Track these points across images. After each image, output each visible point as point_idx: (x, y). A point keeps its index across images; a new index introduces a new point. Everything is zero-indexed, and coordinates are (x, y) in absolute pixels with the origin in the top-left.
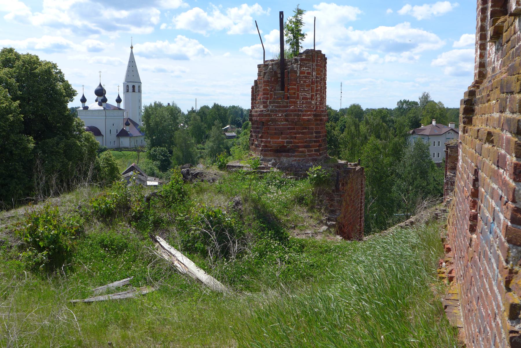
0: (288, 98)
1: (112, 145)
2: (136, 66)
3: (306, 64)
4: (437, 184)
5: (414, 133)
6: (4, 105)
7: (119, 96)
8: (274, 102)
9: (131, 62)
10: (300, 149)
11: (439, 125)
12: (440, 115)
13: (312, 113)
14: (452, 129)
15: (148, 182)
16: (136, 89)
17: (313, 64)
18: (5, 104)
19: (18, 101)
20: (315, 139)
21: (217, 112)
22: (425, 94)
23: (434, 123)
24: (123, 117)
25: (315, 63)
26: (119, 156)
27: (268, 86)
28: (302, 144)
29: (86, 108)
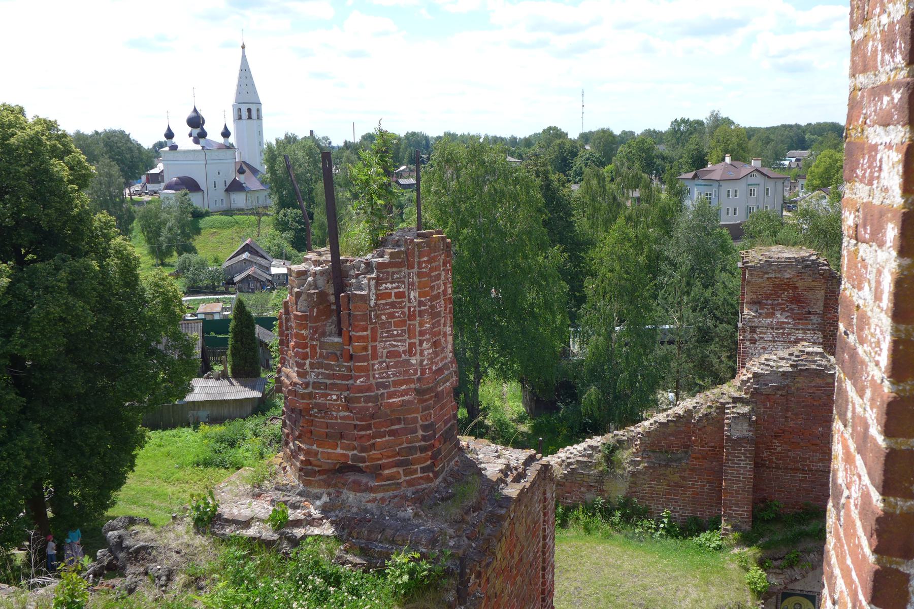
0: (351, 357)
1: (220, 206)
2: (251, 77)
3: (393, 273)
4: (729, 294)
5: (695, 176)
7: (226, 128)
8: (320, 366)
10: (387, 472)
11: (736, 163)
12: (738, 145)
13: (413, 386)
14: (757, 170)
17: (409, 274)
20: (423, 443)
22: (715, 114)
23: (728, 160)
24: (234, 161)
25: (416, 270)
27: (305, 328)
28: (391, 460)
29: (174, 148)
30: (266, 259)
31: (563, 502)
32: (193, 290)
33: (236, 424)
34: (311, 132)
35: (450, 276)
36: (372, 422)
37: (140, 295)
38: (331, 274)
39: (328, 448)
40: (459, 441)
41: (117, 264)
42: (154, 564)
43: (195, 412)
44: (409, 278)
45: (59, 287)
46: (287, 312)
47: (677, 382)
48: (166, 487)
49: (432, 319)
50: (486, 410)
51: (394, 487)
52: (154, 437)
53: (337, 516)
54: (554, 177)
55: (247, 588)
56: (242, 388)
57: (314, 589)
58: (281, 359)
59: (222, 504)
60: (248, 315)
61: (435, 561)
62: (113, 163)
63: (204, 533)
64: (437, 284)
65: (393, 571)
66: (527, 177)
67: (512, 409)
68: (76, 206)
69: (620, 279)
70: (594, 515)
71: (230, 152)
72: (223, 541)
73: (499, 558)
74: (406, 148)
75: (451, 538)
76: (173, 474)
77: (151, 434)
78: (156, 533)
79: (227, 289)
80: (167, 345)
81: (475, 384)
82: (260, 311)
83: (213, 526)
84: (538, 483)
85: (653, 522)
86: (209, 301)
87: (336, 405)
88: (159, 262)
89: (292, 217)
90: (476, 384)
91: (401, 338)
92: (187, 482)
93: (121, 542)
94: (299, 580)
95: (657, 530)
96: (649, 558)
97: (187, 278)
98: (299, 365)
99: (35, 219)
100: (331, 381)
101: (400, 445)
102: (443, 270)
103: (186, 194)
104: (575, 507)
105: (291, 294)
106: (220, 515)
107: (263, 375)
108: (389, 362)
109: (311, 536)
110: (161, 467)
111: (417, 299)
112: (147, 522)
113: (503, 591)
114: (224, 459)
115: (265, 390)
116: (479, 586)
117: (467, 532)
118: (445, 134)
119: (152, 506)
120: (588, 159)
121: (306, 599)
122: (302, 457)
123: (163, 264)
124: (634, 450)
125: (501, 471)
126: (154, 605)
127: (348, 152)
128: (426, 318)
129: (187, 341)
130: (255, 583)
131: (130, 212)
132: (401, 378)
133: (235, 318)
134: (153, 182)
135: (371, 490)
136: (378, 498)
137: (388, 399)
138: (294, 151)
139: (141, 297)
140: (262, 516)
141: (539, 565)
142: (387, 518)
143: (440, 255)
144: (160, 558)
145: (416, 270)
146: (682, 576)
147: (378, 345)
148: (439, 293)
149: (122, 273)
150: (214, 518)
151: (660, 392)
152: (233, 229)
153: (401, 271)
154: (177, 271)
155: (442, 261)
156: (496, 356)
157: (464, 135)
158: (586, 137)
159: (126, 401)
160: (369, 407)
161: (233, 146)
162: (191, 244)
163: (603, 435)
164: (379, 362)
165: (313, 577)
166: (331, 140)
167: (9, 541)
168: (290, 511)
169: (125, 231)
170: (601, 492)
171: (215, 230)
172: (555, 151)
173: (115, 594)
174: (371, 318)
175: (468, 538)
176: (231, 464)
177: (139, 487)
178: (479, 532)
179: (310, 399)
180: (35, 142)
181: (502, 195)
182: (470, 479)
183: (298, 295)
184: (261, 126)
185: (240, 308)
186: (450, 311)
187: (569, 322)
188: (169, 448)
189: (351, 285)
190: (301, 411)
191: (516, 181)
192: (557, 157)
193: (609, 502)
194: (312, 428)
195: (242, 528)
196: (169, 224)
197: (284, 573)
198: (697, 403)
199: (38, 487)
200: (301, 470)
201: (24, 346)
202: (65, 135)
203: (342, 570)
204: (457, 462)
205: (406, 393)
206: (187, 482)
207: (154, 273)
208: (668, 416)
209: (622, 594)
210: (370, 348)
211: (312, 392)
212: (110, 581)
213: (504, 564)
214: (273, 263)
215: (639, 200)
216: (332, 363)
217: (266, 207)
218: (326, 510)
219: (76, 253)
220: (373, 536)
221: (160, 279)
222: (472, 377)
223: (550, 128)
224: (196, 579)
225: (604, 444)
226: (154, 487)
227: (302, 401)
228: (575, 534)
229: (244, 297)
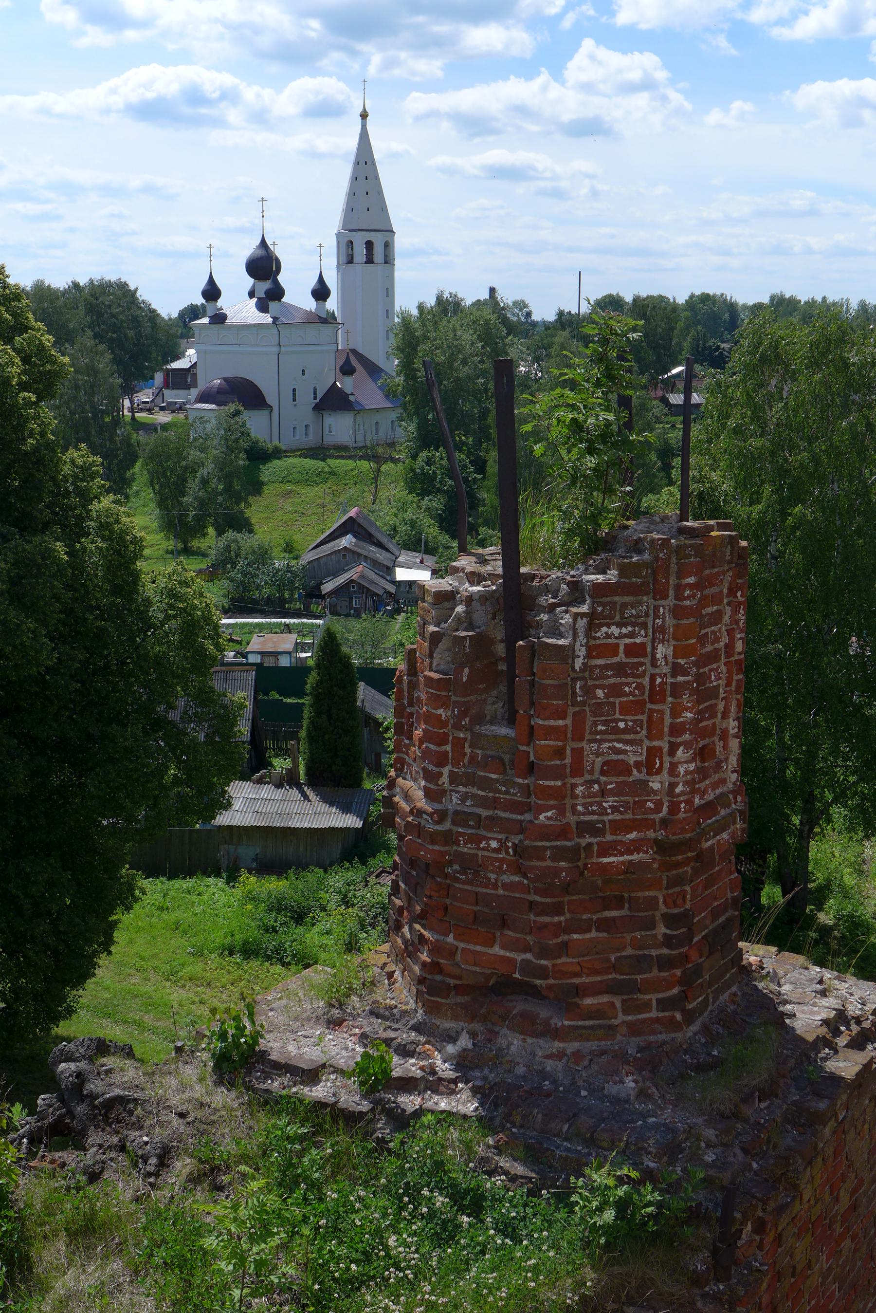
0: (531, 769)
2: (377, 177)
3: (624, 606)
7: (321, 279)
8: (470, 780)
9: (362, 163)
10: (588, 1001)
13: (651, 834)
15: (398, 570)
17: (657, 608)
20: (665, 951)
24: (334, 347)
25: (670, 601)
26: (318, 475)
27: (445, 705)
28: (599, 979)
29: (219, 318)
30: (387, 550)
33: (310, 877)
34: (492, 291)
35: (741, 616)
36: (566, 899)
37: (141, 613)
38: (501, 601)
39: (476, 944)
40: (740, 954)
41: (100, 549)
42: (137, 1133)
43: (232, 848)
44: (656, 616)
46: (412, 670)
48: (169, 991)
49: (699, 702)
50: (820, 897)
53: (485, 1078)
55: (305, 1199)
56: (323, 807)
57: (432, 1215)
58: (397, 760)
59: (269, 1032)
61: (672, 1189)
62: (102, 347)
63: (231, 1085)
64: (712, 632)
65: (586, 1199)
68: (31, 434)
71: (327, 329)
72: (266, 1103)
73: (806, 1198)
74: (687, 328)
75: (708, 1146)
76: (183, 965)
77: (145, 883)
78: (144, 1074)
79: (307, 607)
80: (185, 713)
82: (369, 654)
83: (249, 1073)
86: (271, 629)
87: (497, 859)
88: (180, 546)
89: (442, 467)
90: (805, 835)
91: (632, 737)
92: (209, 984)
94: (404, 1194)
97: (231, 580)
98: (429, 776)
100: (490, 813)
101: (618, 950)
102: (729, 604)
103: (237, 413)
106: (264, 1054)
107: (367, 785)
108: (606, 783)
109: (432, 1112)
110: (162, 950)
111: (670, 660)
112: (128, 1052)
113: (809, 1266)
114: (281, 944)
115: (369, 815)
116: (760, 1247)
118: (772, 298)
119: (140, 1025)
121: (415, 1234)
122: (425, 957)
123: (187, 551)
125: (826, 1022)
126: (133, 1207)
127: (566, 333)
129: (225, 707)
130: (320, 1190)
131: (129, 445)
132: (629, 816)
133: (318, 666)
134: (176, 386)
135: (556, 1034)
136: (569, 1052)
137: (599, 856)
139: (143, 616)
140: (341, 1063)
142: (584, 1093)
143: (724, 573)
145: (670, 601)
147: (586, 747)
148: (717, 650)
150: (252, 1057)
152: (324, 487)
153: (641, 603)
154: (213, 566)
155: (726, 585)
156: (852, 779)
157: (814, 302)
159: (104, 818)
160: (562, 869)
161: (334, 318)
162: (242, 513)
164: (586, 782)
165: (431, 1191)
166: (533, 307)
168: (395, 1059)
171: (290, 487)
173: (65, 1178)
175: (745, 1151)
176: (294, 956)
177: (118, 986)
178: (768, 1141)
179: (446, 844)
182: (759, 1032)
183: (435, 639)
186: (738, 687)
188: (177, 915)
189: (539, 625)
190: (427, 865)
194: (448, 902)
195: (303, 1083)
196: (203, 472)
197: (377, 1178)
200: (421, 981)
202: (17, 294)
203: (488, 1186)
204: (735, 995)
205: (636, 847)
206: (209, 984)
207: (170, 570)
210: (568, 752)
211: (450, 830)
212: (57, 1155)
214: (401, 559)
216: (494, 776)
217: (392, 445)
220: (553, 1125)
221: (180, 582)
222: (796, 820)
224: (212, 1170)
226: (147, 989)
227: (430, 847)
229: (339, 626)
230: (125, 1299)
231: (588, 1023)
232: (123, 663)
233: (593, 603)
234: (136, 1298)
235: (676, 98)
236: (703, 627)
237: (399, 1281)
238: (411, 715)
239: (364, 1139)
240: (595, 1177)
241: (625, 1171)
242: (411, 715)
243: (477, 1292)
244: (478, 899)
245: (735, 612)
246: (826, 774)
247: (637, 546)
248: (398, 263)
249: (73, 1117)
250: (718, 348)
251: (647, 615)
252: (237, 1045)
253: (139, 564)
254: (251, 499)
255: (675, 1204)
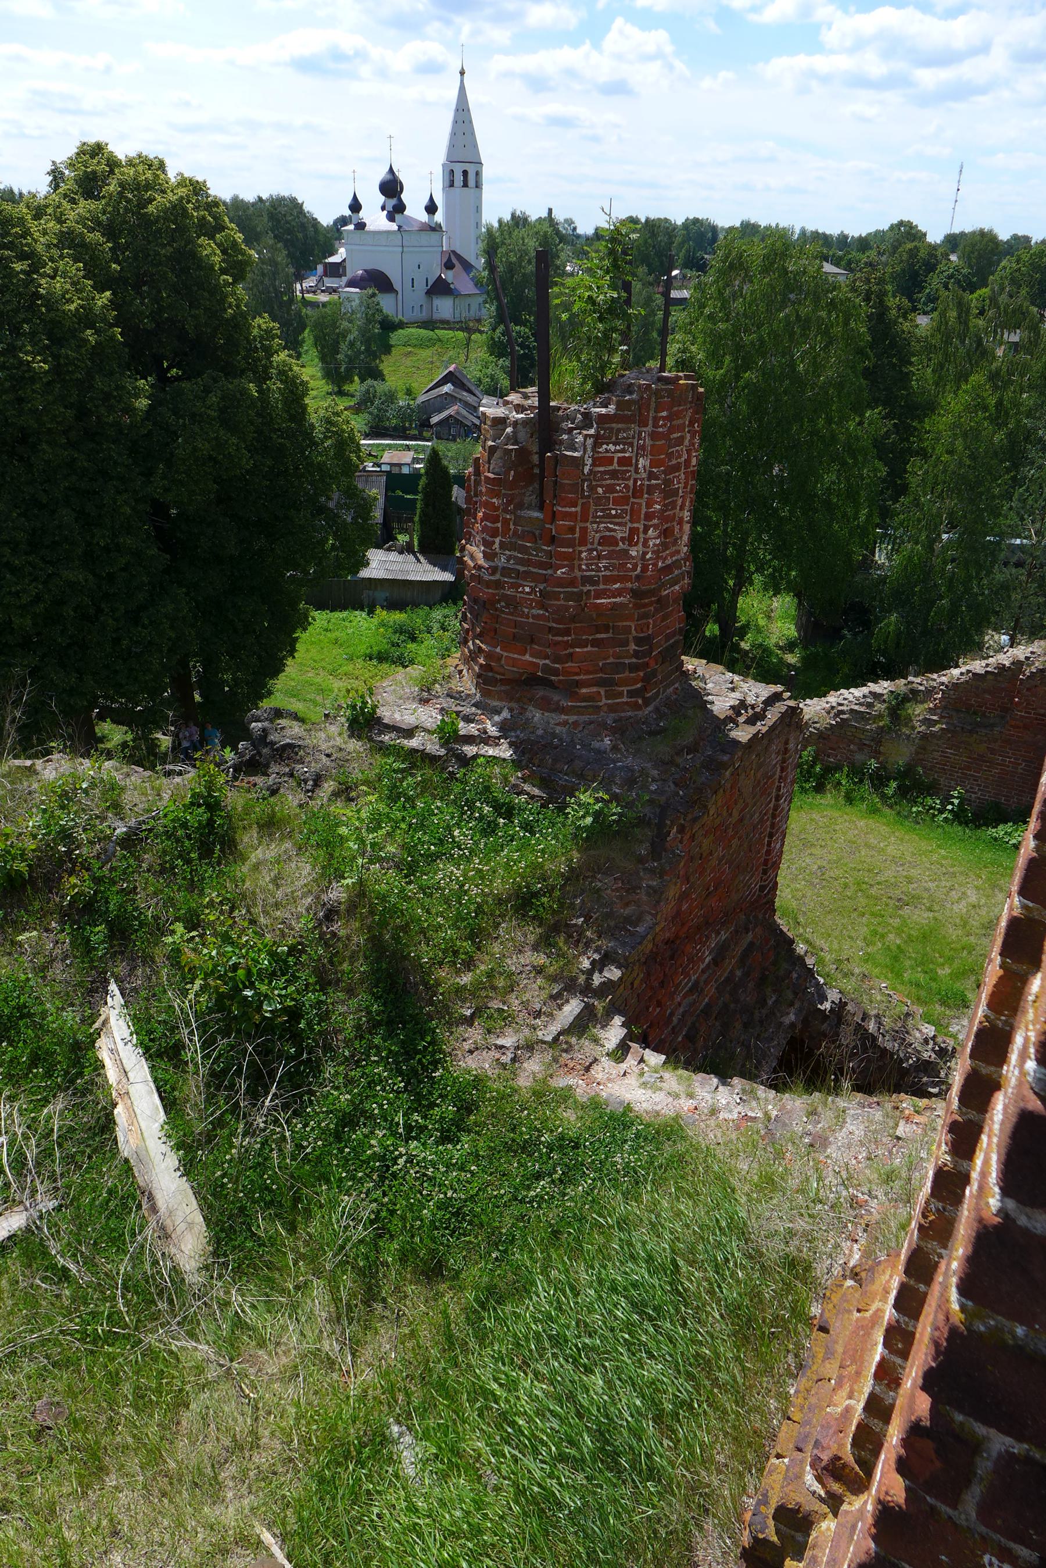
0: (552, 540)
2: (471, 122)
3: (619, 431)
6: (72, 307)
7: (431, 198)
8: (513, 547)
9: (460, 122)
10: (584, 690)
13: (629, 585)
16: (471, 182)
17: (640, 433)
18: (75, 304)
19: (108, 293)
20: (634, 660)
21: (649, 241)
27: (497, 495)
29: (361, 226)
30: (474, 395)
31: (823, 760)
32: (377, 431)
33: (421, 612)
34: (550, 211)
35: (697, 440)
36: (572, 626)
41: (280, 388)
43: (371, 593)
44: (639, 439)
45: (208, 416)
46: (477, 472)
47: (1017, 621)
49: (665, 498)
50: (742, 632)
51: (591, 710)
52: (320, 618)
53: (517, 737)
54: (892, 302)
55: (404, 807)
56: (430, 567)
57: (481, 818)
60: (445, 470)
61: (629, 805)
62: (280, 245)
63: (359, 738)
66: (849, 299)
67: (780, 632)
69: (961, 464)
70: (861, 781)
71: (434, 236)
72: (381, 749)
73: (711, 813)
74: (683, 243)
75: (653, 781)
77: (316, 614)
79: (421, 433)
81: (734, 593)
82: (461, 467)
84: (779, 728)
85: (938, 802)
86: (396, 447)
88: (336, 389)
90: (736, 592)
91: (620, 520)
93: (266, 736)
95: (941, 812)
96: (924, 845)
97: (370, 413)
98: (487, 544)
99: (180, 321)
101: (605, 659)
102: (689, 432)
103: (374, 295)
104: (838, 768)
105: (484, 447)
109: (484, 756)
111: (647, 468)
112: (295, 717)
113: (711, 854)
116: (681, 842)
117: (676, 776)
118: (742, 222)
120: (950, 277)
121: (471, 829)
122: (482, 661)
123: (341, 393)
124: (931, 705)
125: (732, 707)
126: (298, 810)
128: (657, 496)
129: (363, 499)
130: (413, 802)
131: (300, 317)
132: (616, 573)
133: (426, 473)
135: (563, 710)
138: (523, 239)
141: (765, 830)
142: (578, 747)
144: (307, 760)
146: (961, 873)
147: (590, 526)
149: (285, 401)
151: (990, 632)
153: (629, 429)
156: (768, 557)
158: (953, 241)
160: (571, 606)
161: (441, 227)
162: (377, 367)
163: (893, 680)
164: (589, 550)
167: (151, 723)
168: (461, 724)
169: (293, 344)
170: (876, 754)
172: (902, 261)
174: (583, 489)
175: (676, 784)
179: (496, 589)
180: (178, 211)
181: (806, 324)
182: (690, 712)
183: (492, 450)
184: (479, 198)
185: (434, 460)
186: (692, 489)
187: (878, 521)
188: (337, 634)
189: (561, 442)
191: (832, 305)
192: (903, 270)
193: (885, 768)
195: (404, 737)
196: (351, 337)
198: (1032, 653)
199: (184, 664)
200: (479, 676)
201: (167, 490)
202: (216, 203)
204: (677, 689)
205: (619, 593)
208: (987, 665)
209: (878, 883)
212: (251, 779)
213: (718, 822)
214: (483, 401)
215: (1015, 347)
217: (479, 321)
218: (505, 728)
219: (230, 371)
221: (333, 413)
222: (731, 583)
223: (901, 223)
224: (347, 789)
225: (891, 692)
228: (832, 802)
229: (441, 447)
230: (293, 865)
231: (583, 704)
232: (297, 468)
233: (598, 427)
234: (300, 864)
235: (678, 65)
236: (670, 447)
237: (460, 856)
238: (476, 503)
239: (441, 772)
240: (582, 797)
241: (601, 794)
242: (476, 503)
243: (507, 863)
244: (516, 624)
245: (693, 437)
246: (752, 554)
247: (629, 389)
248: (485, 187)
249: (261, 756)
250: (703, 258)
251: (633, 437)
252: (363, 713)
253: (307, 401)
254: (383, 357)
255: (629, 815)
